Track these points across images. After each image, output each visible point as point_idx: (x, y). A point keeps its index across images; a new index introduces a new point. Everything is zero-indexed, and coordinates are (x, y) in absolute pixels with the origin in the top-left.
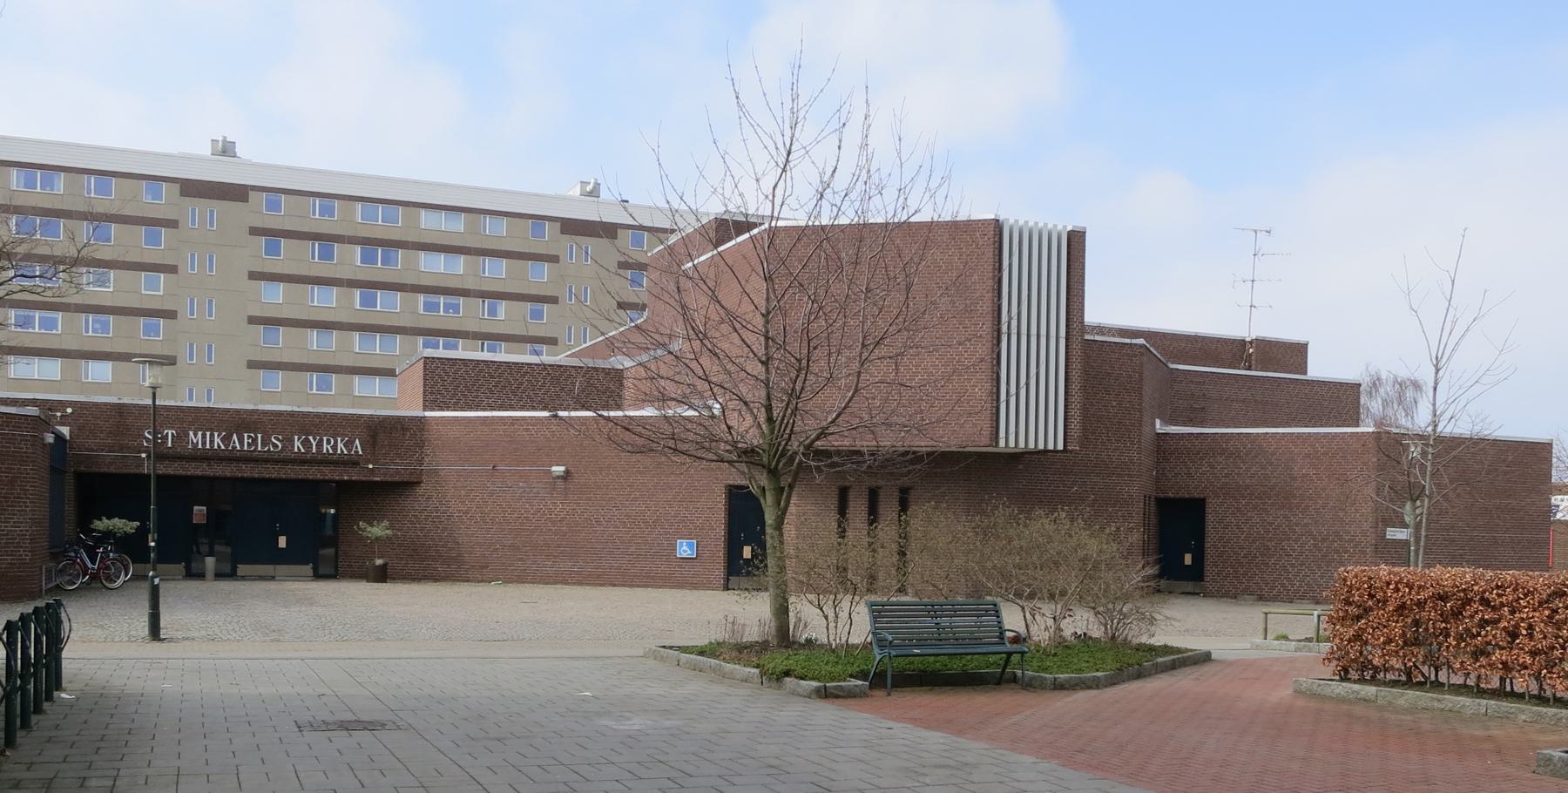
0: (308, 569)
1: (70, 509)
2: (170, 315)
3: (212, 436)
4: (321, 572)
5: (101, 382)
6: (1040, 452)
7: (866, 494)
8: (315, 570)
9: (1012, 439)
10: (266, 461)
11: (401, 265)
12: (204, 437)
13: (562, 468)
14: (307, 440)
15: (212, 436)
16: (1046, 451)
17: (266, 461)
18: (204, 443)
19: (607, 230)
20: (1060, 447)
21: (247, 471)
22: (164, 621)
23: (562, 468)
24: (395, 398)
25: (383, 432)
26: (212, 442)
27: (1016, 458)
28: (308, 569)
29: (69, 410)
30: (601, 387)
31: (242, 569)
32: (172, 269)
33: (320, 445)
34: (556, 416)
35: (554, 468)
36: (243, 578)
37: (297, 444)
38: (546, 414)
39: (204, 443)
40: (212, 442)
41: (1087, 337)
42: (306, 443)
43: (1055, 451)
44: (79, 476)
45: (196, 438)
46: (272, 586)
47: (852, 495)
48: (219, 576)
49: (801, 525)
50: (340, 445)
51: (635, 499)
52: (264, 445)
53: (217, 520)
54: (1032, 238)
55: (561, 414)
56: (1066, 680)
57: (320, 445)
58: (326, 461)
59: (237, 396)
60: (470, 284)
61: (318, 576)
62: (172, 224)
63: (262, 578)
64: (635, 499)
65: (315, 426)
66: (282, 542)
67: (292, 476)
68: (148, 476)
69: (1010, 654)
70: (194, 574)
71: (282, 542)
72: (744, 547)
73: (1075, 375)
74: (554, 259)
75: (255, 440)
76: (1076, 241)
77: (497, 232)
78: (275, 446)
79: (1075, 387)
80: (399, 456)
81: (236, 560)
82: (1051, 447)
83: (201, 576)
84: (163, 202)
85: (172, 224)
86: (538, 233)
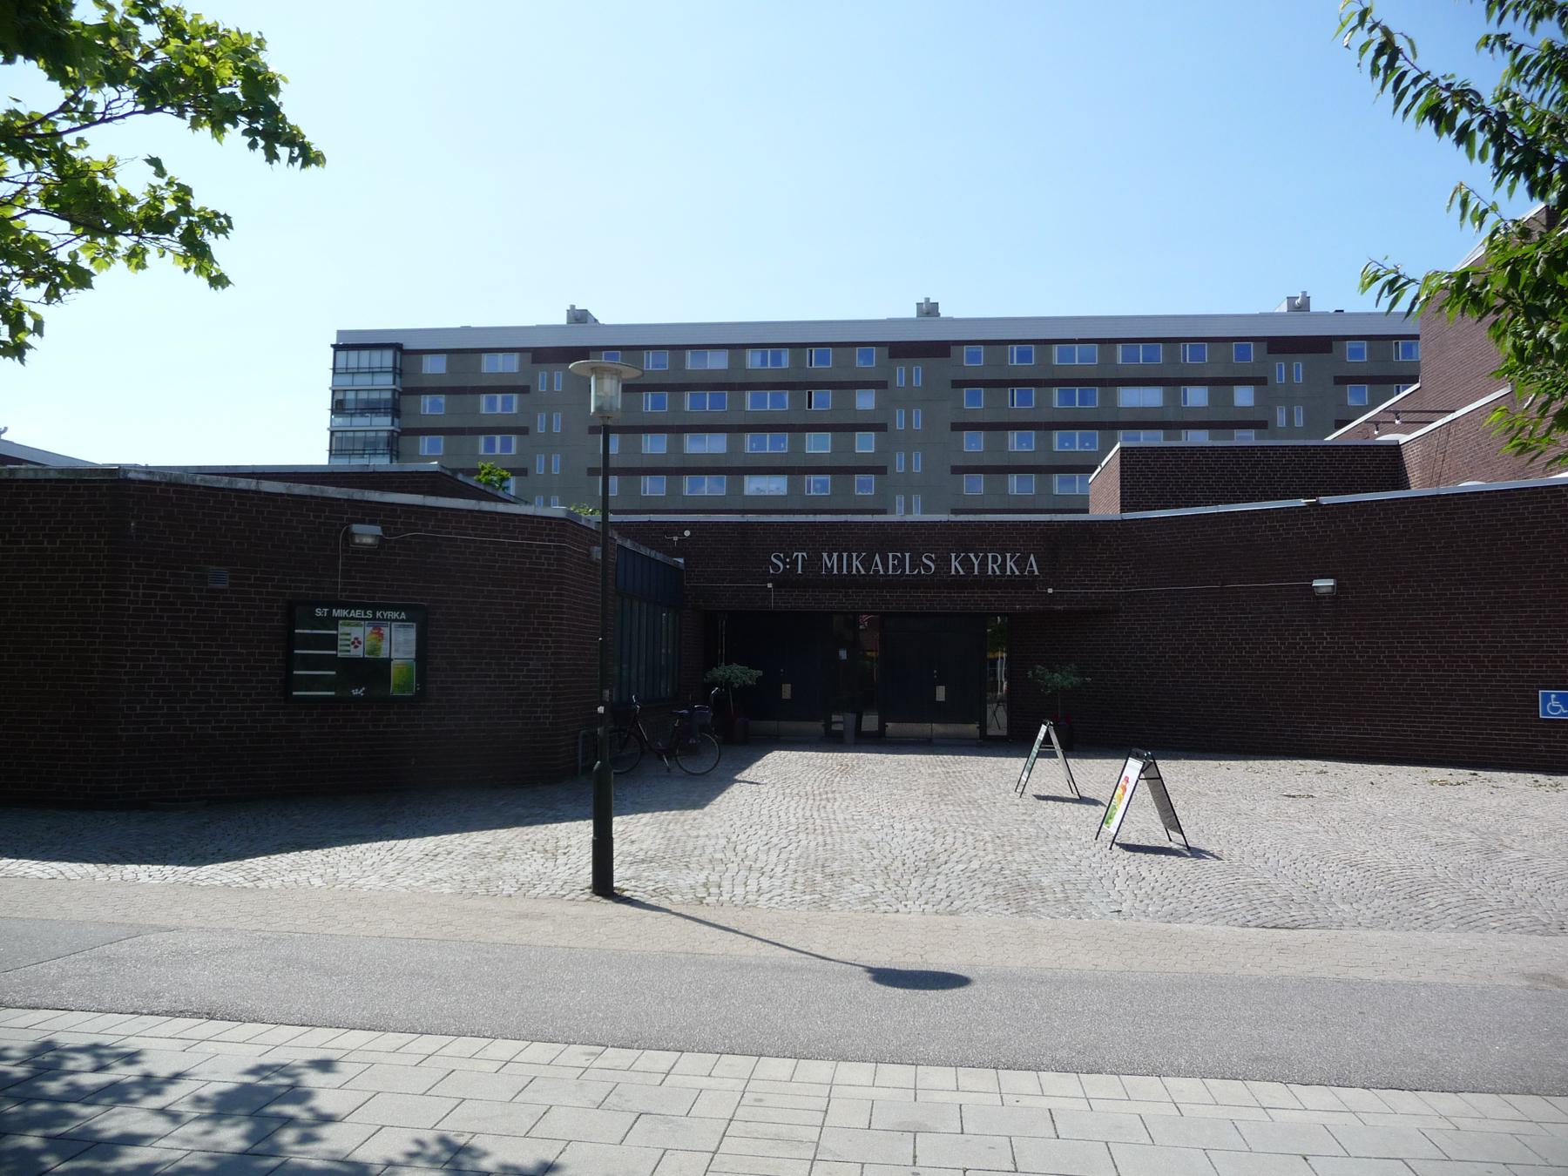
3: (850, 558)
12: (840, 559)
15: (850, 558)
18: (840, 568)
26: (850, 565)
29: (687, 533)
39: (840, 568)
40: (850, 565)
42: (868, 563)
55: (1325, 500)
57: (984, 564)
66: (941, 693)
71: (941, 693)
78: (776, 567)
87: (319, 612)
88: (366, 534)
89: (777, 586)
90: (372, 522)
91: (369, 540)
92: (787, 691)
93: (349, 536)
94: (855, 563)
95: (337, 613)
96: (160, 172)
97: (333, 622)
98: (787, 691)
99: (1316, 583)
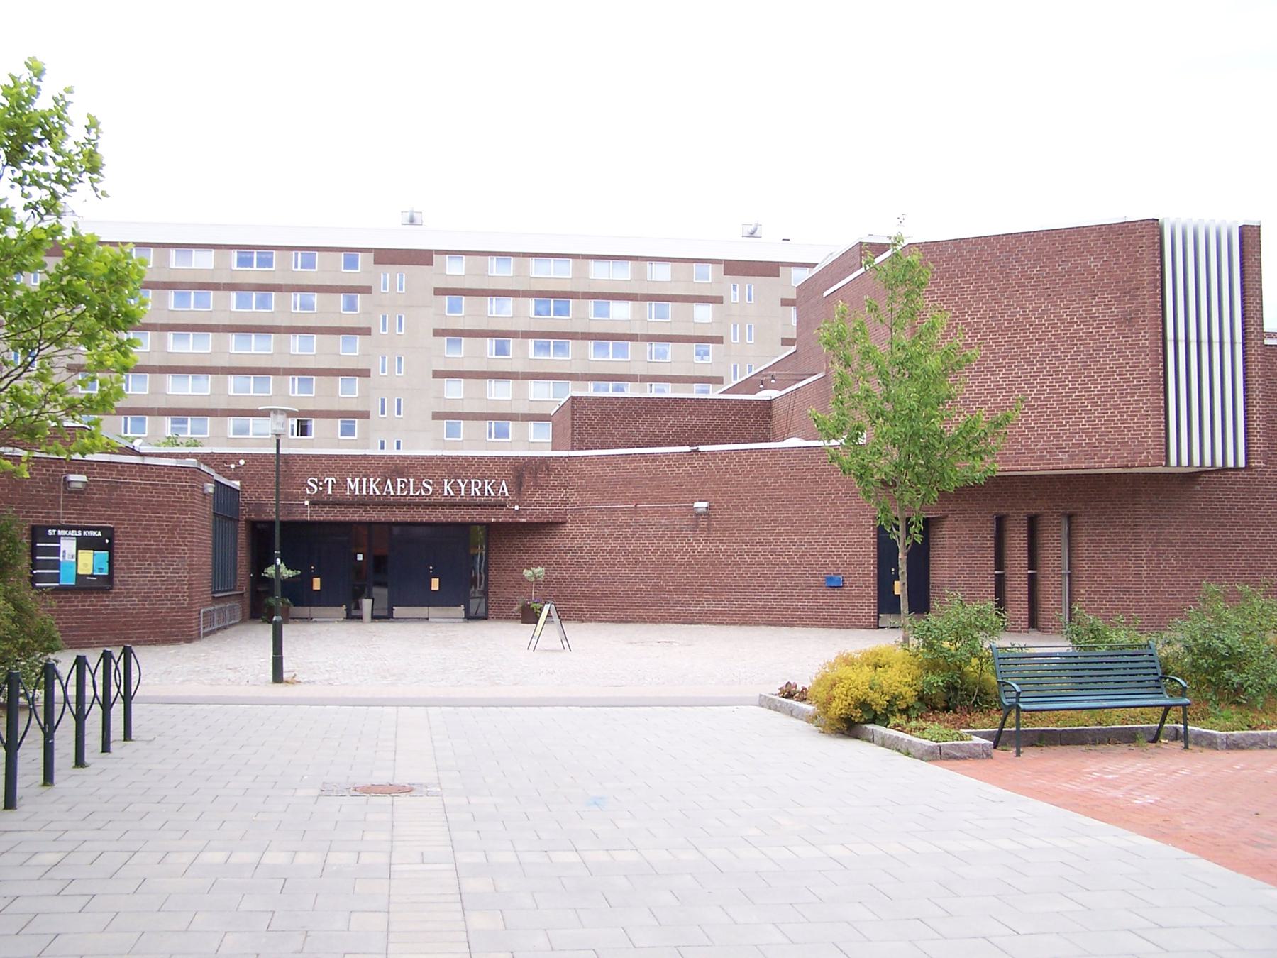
0: (460, 611)
1: (244, 558)
2: (365, 373)
3: (368, 482)
4: (472, 611)
5: (256, 438)
6: (1218, 471)
7: (1025, 523)
8: (466, 611)
9: (1184, 454)
10: (418, 505)
11: (585, 315)
12: (361, 483)
13: (705, 504)
14: (456, 483)
15: (368, 482)
16: (1225, 469)
17: (418, 505)
18: (361, 490)
19: (422, 258)
20: (1242, 463)
21: (400, 515)
22: (287, 665)
23: (705, 504)
24: (536, 442)
25: (525, 473)
26: (368, 487)
27: (1191, 478)
28: (460, 611)
29: (242, 462)
30: (755, 420)
31: (398, 611)
32: (366, 331)
33: (468, 487)
34: (83, 455)
35: (697, 504)
36: (399, 620)
37: (447, 487)
38: (687, 449)
39: (361, 490)
40: (368, 487)
41: (1267, 342)
42: (381, 485)
43: (1236, 469)
44: (253, 526)
45: (353, 485)
46: (312, 628)
47: (1009, 524)
48: (375, 618)
49: (959, 561)
50: (487, 487)
51: (779, 534)
52: (416, 489)
53: (379, 563)
54: (1196, 238)
55: (702, 448)
56: (1242, 738)
57: (468, 487)
58: (384, 503)
59: (425, 443)
60: (637, 329)
61: (469, 617)
62: (367, 290)
63: (420, 619)
64: (779, 534)
65: (464, 468)
66: (435, 584)
67: (443, 519)
68: (272, 523)
69: (1168, 707)
70: (353, 616)
71: (435, 584)
72: (902, 580)
73: (1256, 383)
74: (717, 300)
75: (407, 484)
76: (1249, 238)
77: (661, 275)
78: (311, 489)
79: (1256, 395)
80: (543, 496)
81: (395, 601)
82: (1230, 464)
83: (360, 618)
84: (706, 280)
85: (367, 290)
86: (352, 263)
87: (51, 532)
88: (78, 479)
89: (313, 504)
90: (80, 473)
91: (80, 485)
92: (317, 584)
93: (67, 483)
94: (373, 486)
95: (61, 533)
96: (803, 696)
97: (57, 539)
98: (317, 584)
99: (697, 504)
